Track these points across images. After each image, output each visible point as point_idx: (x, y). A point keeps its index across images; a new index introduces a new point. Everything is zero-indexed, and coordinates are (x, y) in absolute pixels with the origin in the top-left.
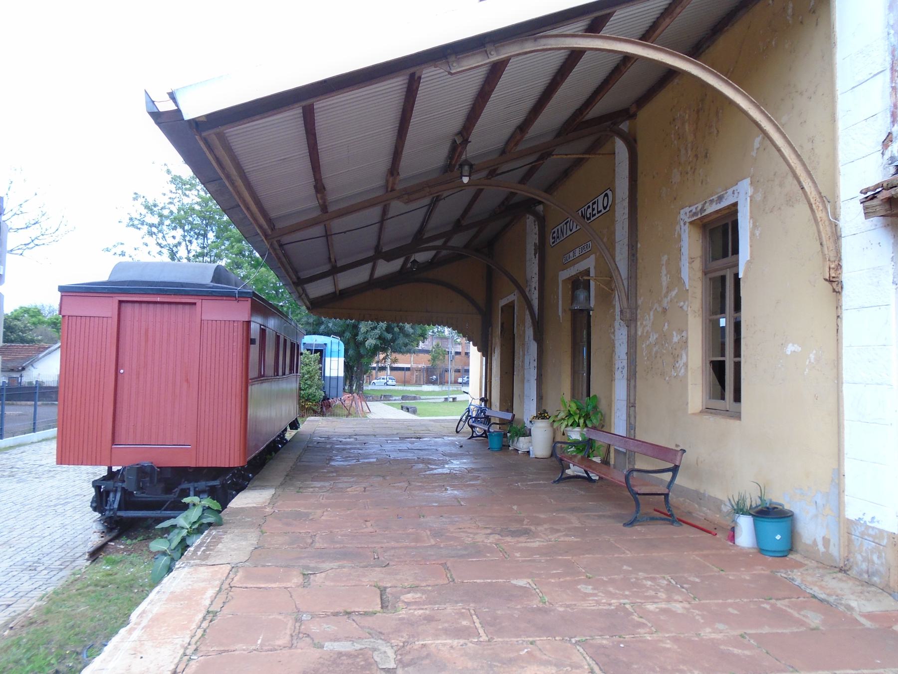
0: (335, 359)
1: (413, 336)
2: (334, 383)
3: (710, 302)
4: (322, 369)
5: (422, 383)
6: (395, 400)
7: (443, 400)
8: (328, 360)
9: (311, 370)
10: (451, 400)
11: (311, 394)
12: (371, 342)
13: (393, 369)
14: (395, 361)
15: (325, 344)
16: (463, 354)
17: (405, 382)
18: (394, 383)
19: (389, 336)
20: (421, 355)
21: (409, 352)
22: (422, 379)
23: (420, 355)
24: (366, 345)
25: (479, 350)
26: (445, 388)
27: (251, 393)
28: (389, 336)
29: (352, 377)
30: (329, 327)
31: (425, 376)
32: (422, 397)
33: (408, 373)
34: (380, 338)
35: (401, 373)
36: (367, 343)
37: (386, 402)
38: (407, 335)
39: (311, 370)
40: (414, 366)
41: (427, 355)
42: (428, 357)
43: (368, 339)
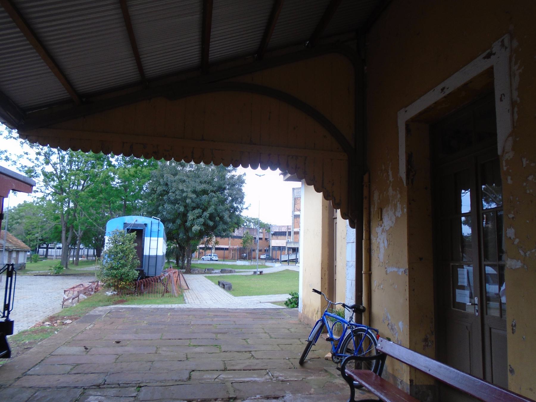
0: (154, 239)
1: (230, 223)
2: (152, 262)
3: (88, 271)
4: (140, 249)
5: (236, 258)
6: (216, 273)
7: (252, 273)
8: (147, 240)
9: (125, 249)
10: (259, 273)
11: (124, 274)
12: (196, 228)
13: (217, 249)
14: (217, 243)
15: (146, 225)
16: (264, 239)
17: (224, 258)
18: (217, 259)
19: (211, 223)
20: (236, 240)
21: (227, 236)
22: (236, 256)
23: (235, 239)
24: (193, 230)
25: (352, 225)
26: (253, 263)
27: (145, 259)
28: (211, 223)
29: (184, 254)
30: (163, 215)
31: (238, 254)
32: (237, 270)
33: (226, 252)
34: (204, 224)
35: (222, 252)
36: (193, 228)
37: (207, 275)
38: (225, 223)
39: (125, 249)
40: (231, 247)
41: (240, 240)
42: (241, 241)
43: (194, 225)
